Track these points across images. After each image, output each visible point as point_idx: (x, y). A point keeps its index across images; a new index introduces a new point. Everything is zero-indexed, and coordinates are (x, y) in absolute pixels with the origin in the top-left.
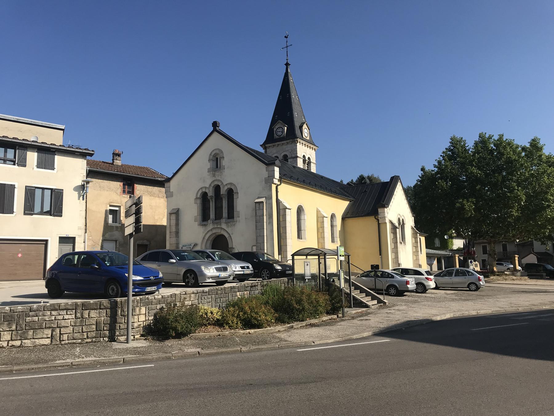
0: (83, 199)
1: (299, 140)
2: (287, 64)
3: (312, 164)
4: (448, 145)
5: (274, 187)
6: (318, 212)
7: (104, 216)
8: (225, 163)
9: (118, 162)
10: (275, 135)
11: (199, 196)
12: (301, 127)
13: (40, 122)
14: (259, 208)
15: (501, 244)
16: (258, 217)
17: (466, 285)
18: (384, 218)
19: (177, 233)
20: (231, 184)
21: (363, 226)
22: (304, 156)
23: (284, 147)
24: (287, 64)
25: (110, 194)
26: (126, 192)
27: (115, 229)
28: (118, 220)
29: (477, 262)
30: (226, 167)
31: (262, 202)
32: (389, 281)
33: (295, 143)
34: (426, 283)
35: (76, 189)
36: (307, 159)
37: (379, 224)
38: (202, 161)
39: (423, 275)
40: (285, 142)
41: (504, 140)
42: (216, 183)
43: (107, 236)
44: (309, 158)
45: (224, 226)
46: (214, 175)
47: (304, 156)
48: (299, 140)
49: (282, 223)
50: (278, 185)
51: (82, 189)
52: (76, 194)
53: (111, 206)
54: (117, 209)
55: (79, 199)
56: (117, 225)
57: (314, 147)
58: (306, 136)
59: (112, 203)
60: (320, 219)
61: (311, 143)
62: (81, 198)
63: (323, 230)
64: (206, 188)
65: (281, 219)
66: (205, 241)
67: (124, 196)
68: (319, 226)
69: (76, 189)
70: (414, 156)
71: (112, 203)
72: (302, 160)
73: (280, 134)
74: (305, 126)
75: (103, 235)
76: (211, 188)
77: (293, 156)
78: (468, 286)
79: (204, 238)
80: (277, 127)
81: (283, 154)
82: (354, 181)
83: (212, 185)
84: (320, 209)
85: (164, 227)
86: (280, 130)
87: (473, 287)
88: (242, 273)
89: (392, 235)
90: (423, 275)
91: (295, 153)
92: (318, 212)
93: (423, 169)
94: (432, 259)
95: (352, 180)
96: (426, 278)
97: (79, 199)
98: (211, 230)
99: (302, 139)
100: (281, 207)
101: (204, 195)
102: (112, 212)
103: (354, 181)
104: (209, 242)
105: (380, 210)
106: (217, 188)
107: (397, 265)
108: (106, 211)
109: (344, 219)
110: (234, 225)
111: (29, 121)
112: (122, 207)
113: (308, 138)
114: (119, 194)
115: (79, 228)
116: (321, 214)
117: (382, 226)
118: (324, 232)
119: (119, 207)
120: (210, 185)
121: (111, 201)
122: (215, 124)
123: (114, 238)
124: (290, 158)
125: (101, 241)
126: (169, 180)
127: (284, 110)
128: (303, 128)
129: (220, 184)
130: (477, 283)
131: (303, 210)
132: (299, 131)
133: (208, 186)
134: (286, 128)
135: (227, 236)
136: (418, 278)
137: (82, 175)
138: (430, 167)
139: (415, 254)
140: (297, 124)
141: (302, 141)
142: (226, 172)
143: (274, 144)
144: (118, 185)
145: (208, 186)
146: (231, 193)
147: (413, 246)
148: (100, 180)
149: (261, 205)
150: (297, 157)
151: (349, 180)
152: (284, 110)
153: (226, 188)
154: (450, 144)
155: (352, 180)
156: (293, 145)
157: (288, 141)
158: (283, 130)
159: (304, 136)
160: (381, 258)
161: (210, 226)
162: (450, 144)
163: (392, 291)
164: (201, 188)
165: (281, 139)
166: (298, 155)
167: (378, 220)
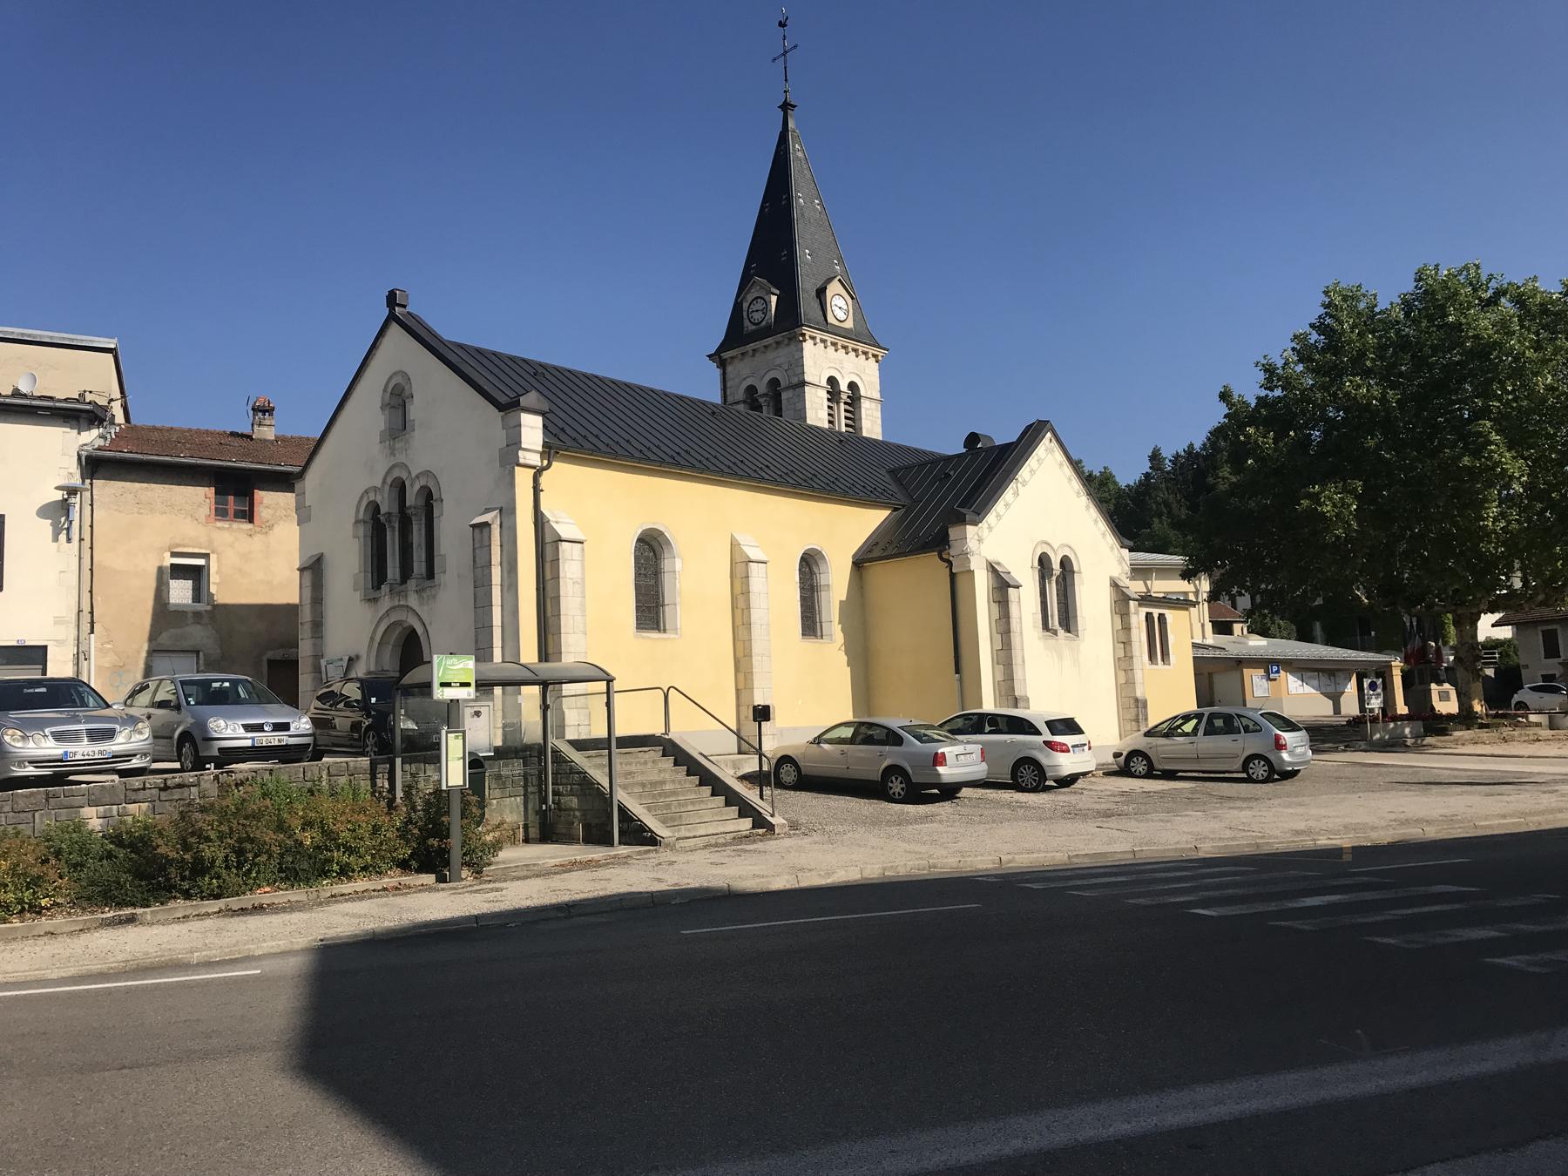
0: (69, 540)
1: (808, 332)
2: (786, 107)
3: (865, 404)
4: (1315, 311)
5: (523, 478)
6: (734, 545)
7: (153, 584)
8: (414, 411)
9: (267, 433)
10: (746, 323)
11: (361, 516)
12: (821, 293)
13: (45, 335)
14: (481, 540)
15: (1540, 628)
16: (479, 571)
17: (1238, 765)
18: (965, 555)
19: (318, 626)
20: (427, 473)
21: (914, 579)
22: (832, 381)
23: (771, 355)
24: (786, 107)
25: (177, 517)
26: (231, 512)
27: (190, 620)
28: (204, 597)
29: (1447, 686)
30: (417, 424)
31: (486, 525)
32: (890, 755)
33: (797, 341)
34: (1045, 758)
35: (46, 511)
36: (844, 387)
37: (953, 576)
38: (367, 410)
39: (1038, 733)
40: (770, 340)
41: (1484, 279)
42: (396, 473)
43: (164, 639)
44: (853, 386)
45: (413, 600)
46: (393, 454)
47: (832, 381)
48: (808, 332)
49: (549, 585)
50: (539, 472)
51: (59, 512)
52: (46, 525)
53: (174, 555)
54: (201, 562)
55: (56, 539)
56: (201, 607)
57: (872, 350)
58: (842, 316)
59: (178, 545)
60: (740, 568)
61: (859, 337)
62: (63, 537)
63: (748, 601)
64: (375, 489)
65: (548, 576)
66: (376, 645)
67: (219, 524)
68: (738, 590)
69: (46, 511)
70: (1203, 356)
71: (178, 545)
72: (823, 395)
73: (757, 316)
74: (834, 288)
75: (152, 638)
76: (387, 488)
77: (795, 380)
78: (1245, 767)
79: (372, 639)
80: (750, 297)
81: (767, 379)
82: (1197, 446)
83: (389, 481)
84: (740, 538)
85: (291, 610)
86: (759, 305)
87: (1260, 770)
88: (248, 743)
89: (995, 607)
90: (1038, 733)
91: (798, 371)
92: (734, 545)
93: (1225, 396)
94: (1341, 676)
95: (1191, 446)
96: (1048, 744)
97: (56, 539)
98: (387, 613)
99: (825, 327)
100: (548, 539)
101: (375, 508)
102: (179, 571)
103: (1197, 446)
104: (388, 650)
105: (953, 532)
106: (400, 487)
107: (1012, 702)
108: (160, 570)
109: (860, 563)
110: (434, 597)
111: (57, 337)
112: (213, 557)
113: (849, 324)
114: (202, 519)
115: (58, 621)
116: (742, 552)
117: (960, 581)
118: (749, 608)
119: (206, 556)
120: (384, 482)
121: (178, 541)
122: (391, 299)
123: (186, 645)
124: (787, 388)
125: (144, 654)
126: (300, 475)
127: (772, 250)
128: (829, 293)
129: (404, 476)
130: (1272, 758)
131: (668, 542)
132: (816, 305)
133: (378, 484)
134: (774, 299)
135: (420, 630)
136: (1024, 744)
137: (64, 472)
138: (1250, 390)
139: (1124, 665)
140: (806, 285)
141: (819, 335)
142: (418, 437)
143: (743, 349)
144: (200, 496)
145: (378, 484)
146: (429, 499)
147: (1116, 641)
148: (137, 485)
149: (486, 530)
150: (803, 384)
151: (1181, 448)
152: (772, 250)
153: (417, 487)
154: (1322, 311)
155: (1191, 446)
156: (793, 347)
157: (778, 337)
158: (767, 303)
159: (831, 319)
160: (961, 680)
161: (386, 603)
162: (1322, 311)
163: (897, 787)
164: (366, 492)
165: (764, 332)
166: (807, 378)
167: (950, 564)
